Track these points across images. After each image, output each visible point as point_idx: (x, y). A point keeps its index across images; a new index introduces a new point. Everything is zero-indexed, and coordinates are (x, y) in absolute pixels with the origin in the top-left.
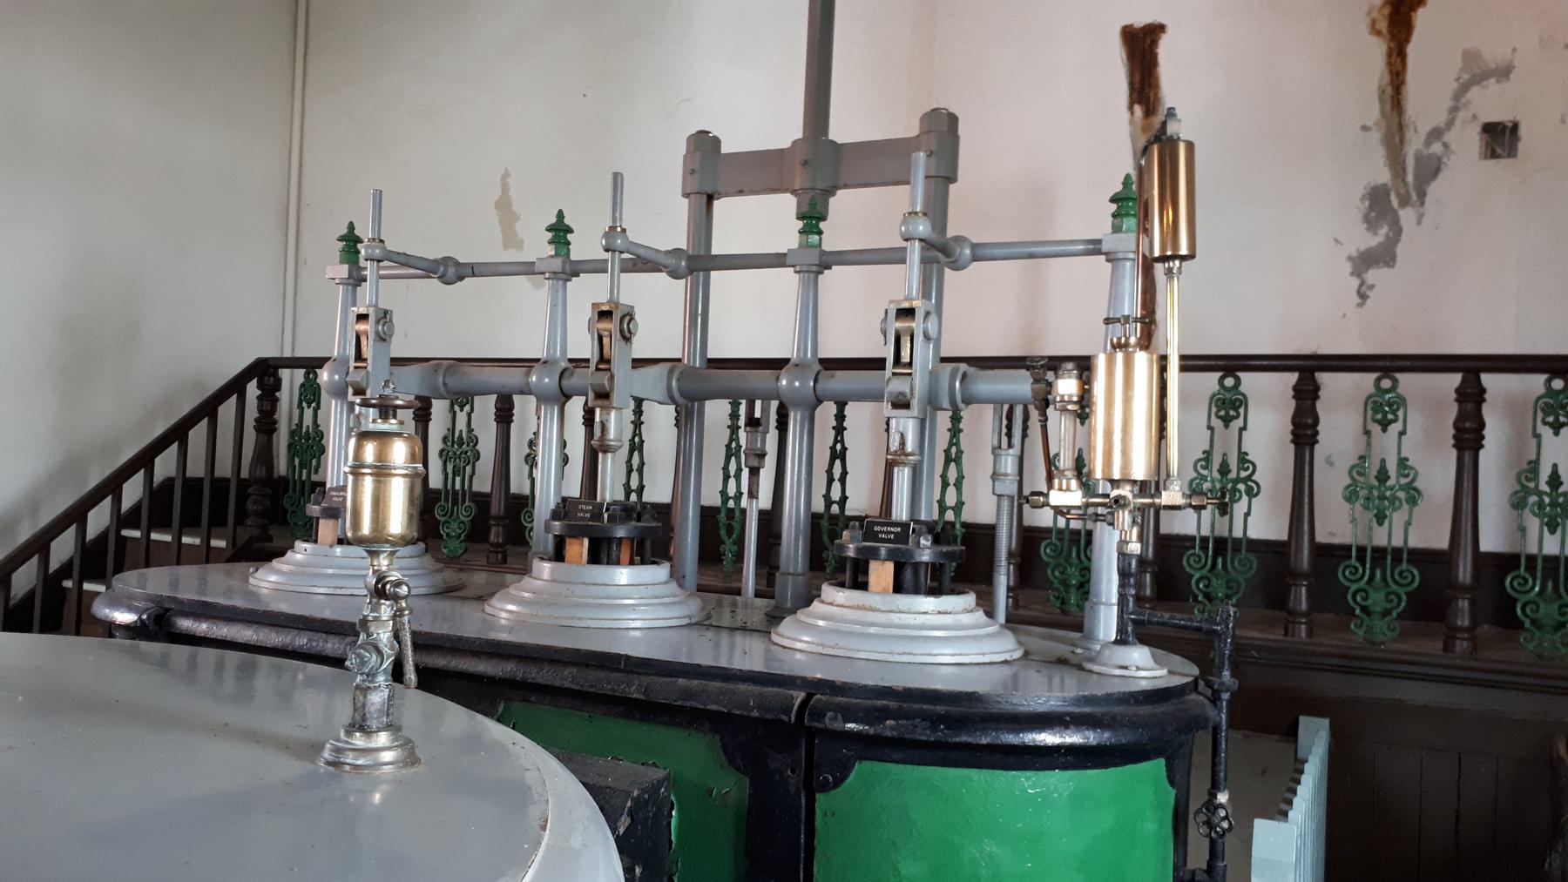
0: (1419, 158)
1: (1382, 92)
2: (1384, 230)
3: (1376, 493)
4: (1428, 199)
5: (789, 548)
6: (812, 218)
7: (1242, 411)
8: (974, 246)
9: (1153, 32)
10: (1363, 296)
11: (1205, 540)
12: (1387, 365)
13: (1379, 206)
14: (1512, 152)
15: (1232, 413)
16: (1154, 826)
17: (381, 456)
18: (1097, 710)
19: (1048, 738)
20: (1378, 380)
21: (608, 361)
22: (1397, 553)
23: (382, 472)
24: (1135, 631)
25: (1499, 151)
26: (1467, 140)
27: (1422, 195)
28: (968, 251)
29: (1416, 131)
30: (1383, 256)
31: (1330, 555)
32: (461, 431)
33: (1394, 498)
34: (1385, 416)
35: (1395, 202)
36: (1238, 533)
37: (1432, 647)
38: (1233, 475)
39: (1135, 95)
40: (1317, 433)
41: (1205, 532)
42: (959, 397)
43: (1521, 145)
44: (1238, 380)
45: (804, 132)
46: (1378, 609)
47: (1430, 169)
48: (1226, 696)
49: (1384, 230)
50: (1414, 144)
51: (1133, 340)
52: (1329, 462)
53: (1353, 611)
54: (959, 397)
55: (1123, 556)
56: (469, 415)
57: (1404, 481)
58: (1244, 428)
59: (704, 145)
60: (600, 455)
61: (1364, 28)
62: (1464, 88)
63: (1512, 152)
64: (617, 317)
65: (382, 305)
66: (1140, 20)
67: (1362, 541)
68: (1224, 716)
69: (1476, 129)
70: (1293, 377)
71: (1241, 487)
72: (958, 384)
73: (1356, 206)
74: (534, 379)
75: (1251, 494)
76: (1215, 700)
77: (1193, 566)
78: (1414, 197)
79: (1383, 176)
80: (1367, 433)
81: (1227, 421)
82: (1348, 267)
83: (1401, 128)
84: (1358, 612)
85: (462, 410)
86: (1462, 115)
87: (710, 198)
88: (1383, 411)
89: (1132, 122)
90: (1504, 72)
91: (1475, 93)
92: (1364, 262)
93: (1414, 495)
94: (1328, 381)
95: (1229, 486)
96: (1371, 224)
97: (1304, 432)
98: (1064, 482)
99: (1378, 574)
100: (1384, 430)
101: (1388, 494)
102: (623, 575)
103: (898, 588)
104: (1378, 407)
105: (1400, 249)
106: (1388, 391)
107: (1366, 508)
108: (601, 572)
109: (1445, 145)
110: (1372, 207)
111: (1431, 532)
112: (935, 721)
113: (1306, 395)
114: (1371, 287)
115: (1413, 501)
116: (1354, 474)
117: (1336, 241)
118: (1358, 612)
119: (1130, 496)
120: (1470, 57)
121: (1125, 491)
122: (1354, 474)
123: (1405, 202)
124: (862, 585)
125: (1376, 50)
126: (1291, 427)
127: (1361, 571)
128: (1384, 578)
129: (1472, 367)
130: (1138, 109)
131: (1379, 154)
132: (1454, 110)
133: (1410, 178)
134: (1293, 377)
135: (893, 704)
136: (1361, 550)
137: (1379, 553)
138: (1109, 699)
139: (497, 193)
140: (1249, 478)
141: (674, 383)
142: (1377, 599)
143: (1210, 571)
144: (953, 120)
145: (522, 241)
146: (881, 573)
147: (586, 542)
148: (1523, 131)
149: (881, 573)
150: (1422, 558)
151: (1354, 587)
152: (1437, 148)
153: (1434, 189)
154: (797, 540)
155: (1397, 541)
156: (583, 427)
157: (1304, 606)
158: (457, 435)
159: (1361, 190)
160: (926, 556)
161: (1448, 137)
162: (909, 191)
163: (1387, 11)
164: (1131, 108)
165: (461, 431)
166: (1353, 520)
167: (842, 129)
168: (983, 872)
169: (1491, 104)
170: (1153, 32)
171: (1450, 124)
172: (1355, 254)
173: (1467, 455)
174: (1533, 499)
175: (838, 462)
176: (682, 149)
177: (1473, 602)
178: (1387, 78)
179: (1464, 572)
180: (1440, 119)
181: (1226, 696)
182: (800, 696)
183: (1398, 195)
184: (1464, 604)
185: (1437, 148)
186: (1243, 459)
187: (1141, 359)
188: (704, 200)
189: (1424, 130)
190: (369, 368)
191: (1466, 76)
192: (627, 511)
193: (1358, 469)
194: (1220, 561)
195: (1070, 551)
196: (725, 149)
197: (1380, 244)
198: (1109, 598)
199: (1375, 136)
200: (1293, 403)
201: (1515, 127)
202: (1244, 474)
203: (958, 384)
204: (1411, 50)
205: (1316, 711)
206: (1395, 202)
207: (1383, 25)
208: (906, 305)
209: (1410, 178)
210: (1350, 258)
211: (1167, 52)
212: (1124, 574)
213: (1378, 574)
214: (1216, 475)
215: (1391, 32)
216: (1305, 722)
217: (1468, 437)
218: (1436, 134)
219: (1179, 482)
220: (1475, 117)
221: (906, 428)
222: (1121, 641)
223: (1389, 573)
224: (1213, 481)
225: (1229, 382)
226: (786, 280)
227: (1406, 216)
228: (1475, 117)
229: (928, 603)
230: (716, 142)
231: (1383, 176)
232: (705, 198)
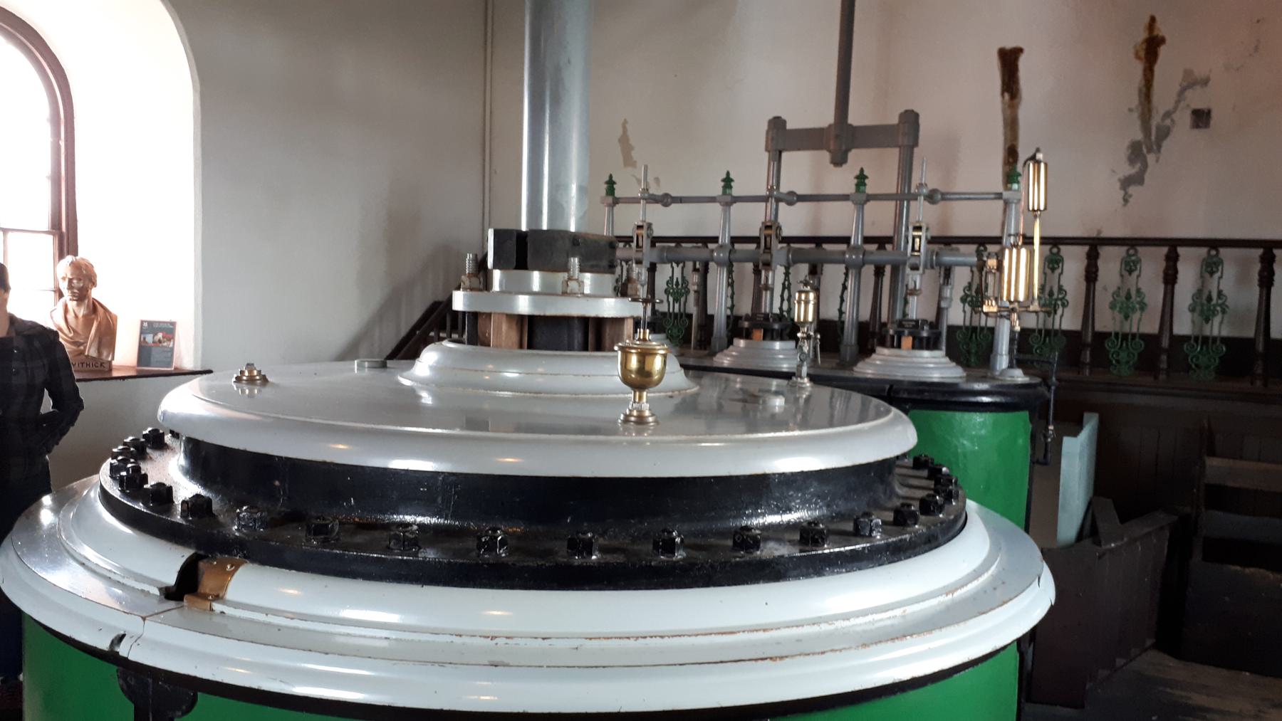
0: (1158, 128)
1: (1140, 91)
2: (1138, 166)
3: (1125, 305)
4: (1163, 149)
5: (848, 336)
6: (862, 178)
7: (1060, 265)
8: (943, 194)
9: (1017, 52)
10: (1126, 200)
11: (1040, 331)
12: (1132, 243)
13: (1136, 153)
14: (1207, 125)
15: (1056, 266)
16: (1023, 441)
17: (807, 297)
18: (1004, 390)
19: (985, 399)
20: (1128, 251)
21: (770, 249)
22: (1134, 336)
23: (807, 302)
24: (1016, 362)
25: (1200, 125)
26: (1184, 118)
27: (1159, 147)
28: (940, 196)
29: (1157, 112)
30: (1137, 179)
31: (1101, 337)
32: (677, 279)
33: (1134, 307)
34: (1131, 268)
35: (1145, 150)
36: (1057, 326)
37: (1149, 380)
38: (1055, 297)
39: (1005, 87)
40: (1097, 276)
41: (1041, 326)
42: (934, 262)
43: (1212, 122)
44: (1059, 250)
45: (835, 119)
46: (1124, 360)
47: (1164, 133)
48: (1053, 388)
49: (1138, 166)
50: (1154, 122)
51: (1020, 243)
52: (1105, 289)
53: (1112, 362)
54: (934, 262)
55: (1012, 332)
56: (683, 268)
57: (1138, 299)
58: (1062, 273)
59: (777, 124)
60: (764, 292)
61: (1131, 55)
62: (1183, 90)
63: (1207, 125)
64: (774, 228)
65: (648, 221)
66: (1009, 44)
67: (1117, 329)
68: (1052, 396)
69: (1188, 112)
70: (1086, 248)
71: (1219, 308)
72: (934, 258)
73: (1123, 152)
74: (715, 254)
75: (1064, 306)
76: (1049, 388)
77: (1035, 343)
78: (1155, 147)
79: (1139, 136)
80: (1122, 276)
81: (1053, 270)
82: (1118, 185)
83: (1150, 111)
84: (1114, 362)
85: (678, 266)
86: (1182, 104)
87: (780, 153)
88: (1130, 266)
89: (1003, 102)
90: (1205, 82)
91: (1189, 93)
92: (1127, 183)
93: (1143, 306)
94: (1105, 251)
95: (1053, 302)
96: (1132, 161)
97: (1091, 275)
98: (990, 302)
99: (1124, 345)
100: (1130, 274)
101: (1131, 305)
102: (777, 345)
103: (914, 347)
104: (1127, 263)
105: (1147, 177)
106: (1133, 255)
107: (1120, 312)
108: (768, 344)
109: (1173, 121)
110: (1132, 153)
111: (1150, 325)
112: (944, 393)
113: (1093, 257)
114: (1131, 196)
115: (1142, 309)
116: (1115, 296)
117: (1114, 171)
118: (1114, 362)
119: (1017, 308)
120: (1188, 73)
121: (1016, 305)
122: (1115, 296)
123: (1150, 151)
124: (899, 346)
125: (1138, 68)
126: (1084, 273)
127: (1116, 343)
128: (1127, 345)
129: (1173, 246)
130: (1007, 96)
131: (1137, 125)
132: (1178, 102)
133: (1153, 138)
134: (1086, 248)
135: (926, 388)
136: (1117, 334)
137: (1125, 336)
138: (1009, 386)
139: (620, 132)
140: (1063, 298)
141: (790, 256)
142: (1123, 356)
143: (1043, 344)
144: (917, 115)
145: (635, 162)
146: (907, 341)
147: (762, 330)
148: (1213, 114)
149: (907, 341)
150: (1144, 337)
151: (1113, 350)
152: (1168, 122)
153: (1166, 144)
154: (852, 330)
155: (1134, 330)
156: (753, 275)
157: (1088, 360)
158: (675, 280)
159: (1127, 143)
160: (925, 334)
161: (1175, 116)
162: (898, 154)
163: (1144, 46)
164: (1003, 94)
165: (677, 279)
166: (1114, 318)
167: (855, 118)
168: (959, 450)
169: (1197, 99)
170: (1017, 52)
171: (1175, 108)
172: (1122, 178)
173: (1169, 287)
174: (969, 299)
175: (786, 291)
176: (765, 127)
177: (1168, 357)
178: (1143, 82)
179: (1165, 343)
180: (1170, 106)
181: (1053, 388)
182: (887, 387)
183: (1147, 147)
184: (1164, 357)
185: (1168, 122)
186: (1061, 289)
187: (1024, 251)
188: (776, 155)
189: (1162, 112)
190: (644, 251)
191: (1185, 84)
192: (780, 317)
193: (1116, 294)
194: (1047, 339)
195: (972, 335)
196: (789, 126)
197: (1137, 173)
198: (1002, 352)
199: (1135, 115)
200: (1086, 261)
201: (1209, 112)
202: (1060, 296)
203: (934, 258)
204: (1157, 68)
205: (1092, 409)
206: (1145, 150)
207: (1142, 54)
208: (918, 225)
209: (1153, 138)
210: (1119, 180)
211: (1023, 63)
212: (1012, 341)
213: (1124, 345)
214: (1047, 296)
215: (1146, 58)
216: (1086, 415)
217: (1170, 278)
218: (1168, 114)
219: (761, 286)
220: (1188, 106)
221: (916, 278)
222: (1011, 366)
223: (1129, 344)
224: (1045, 300)
225: (1055, 250)
226: (849, 206)
227: (1151, 158)
228: (1188, 106)
229: (926, 353)
230: (784, 122)
231: (1139, 136)
232: (778, 153)
